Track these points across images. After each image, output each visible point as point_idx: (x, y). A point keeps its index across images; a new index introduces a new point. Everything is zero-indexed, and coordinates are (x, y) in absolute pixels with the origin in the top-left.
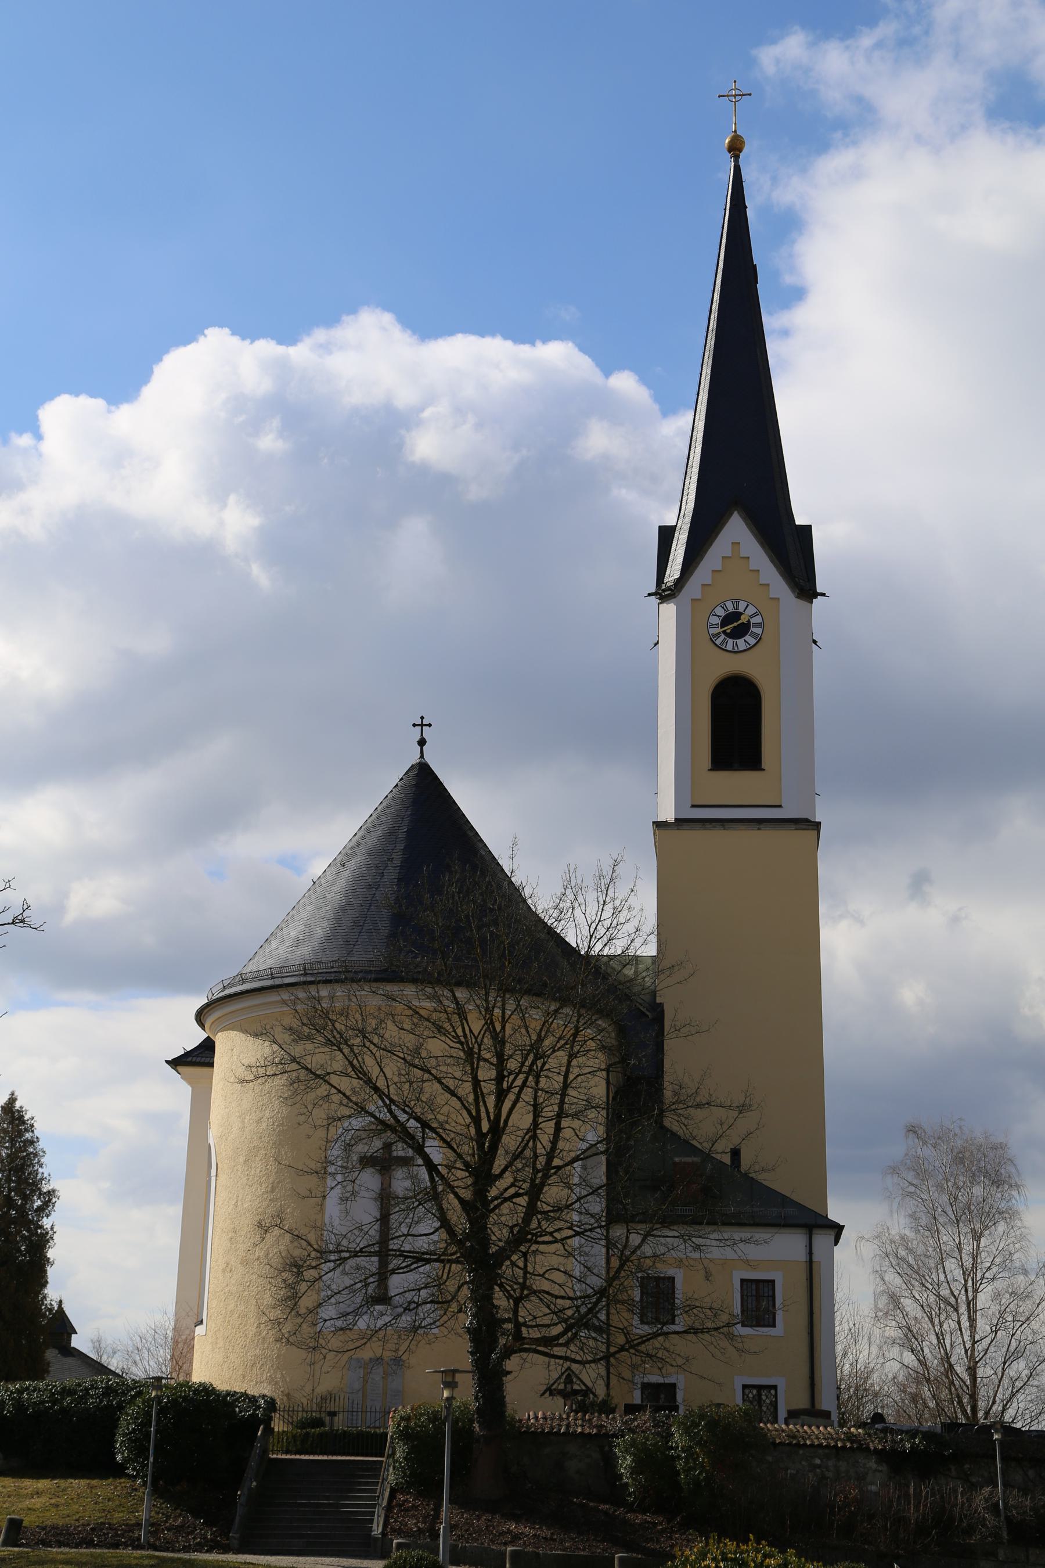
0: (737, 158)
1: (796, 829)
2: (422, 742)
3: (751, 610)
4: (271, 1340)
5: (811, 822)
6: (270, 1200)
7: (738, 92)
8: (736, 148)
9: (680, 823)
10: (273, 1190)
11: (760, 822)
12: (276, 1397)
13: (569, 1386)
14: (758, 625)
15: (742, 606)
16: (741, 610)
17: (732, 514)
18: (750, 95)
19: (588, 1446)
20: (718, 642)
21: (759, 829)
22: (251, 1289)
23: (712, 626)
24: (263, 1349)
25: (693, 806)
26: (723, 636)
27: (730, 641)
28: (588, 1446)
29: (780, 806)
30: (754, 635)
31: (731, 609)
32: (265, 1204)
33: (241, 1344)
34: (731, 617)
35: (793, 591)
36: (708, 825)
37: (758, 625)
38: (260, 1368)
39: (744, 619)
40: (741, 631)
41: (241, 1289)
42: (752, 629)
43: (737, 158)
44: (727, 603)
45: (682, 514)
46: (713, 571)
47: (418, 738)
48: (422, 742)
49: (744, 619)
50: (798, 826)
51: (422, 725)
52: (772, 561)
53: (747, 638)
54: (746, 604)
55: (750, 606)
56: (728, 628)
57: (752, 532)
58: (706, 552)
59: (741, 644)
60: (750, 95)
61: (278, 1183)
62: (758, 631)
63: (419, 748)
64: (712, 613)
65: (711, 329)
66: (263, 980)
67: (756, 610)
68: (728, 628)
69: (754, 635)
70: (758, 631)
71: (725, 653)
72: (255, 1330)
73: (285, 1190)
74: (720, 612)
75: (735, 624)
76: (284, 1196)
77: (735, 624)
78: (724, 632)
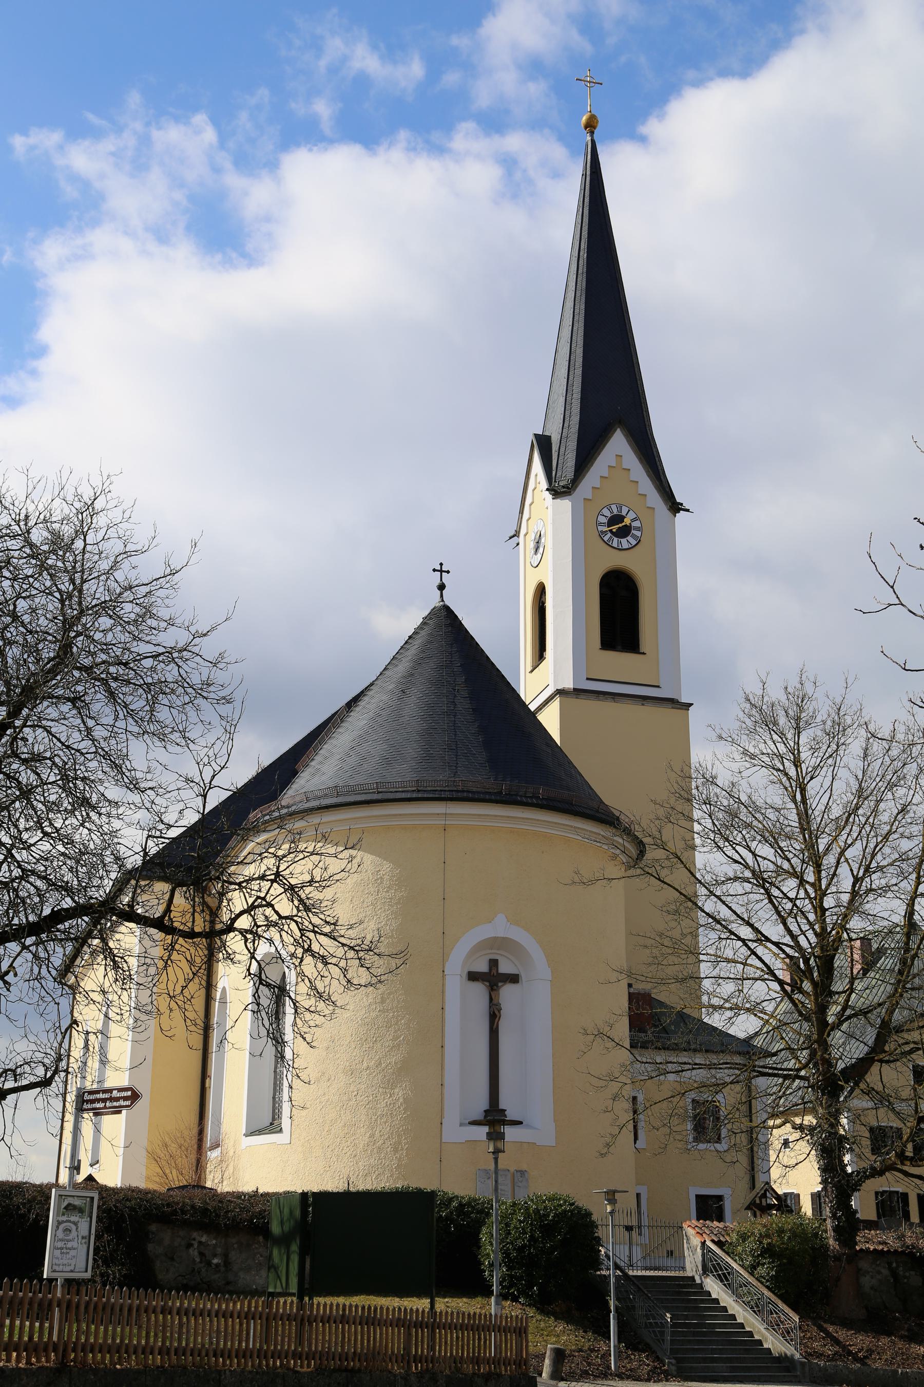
0: (592, 133)
1: (672, 708)
2: (442, 587)
3: (632, 515)
4: (388, 1150)
5: (678, 702)
6: (379, 1011)
7: (592, 80)
8: (591, 125)
9: (577, 692)
10: (383, 1001)
11: (644, 699)
12: (601, 1210)
13: (763, 1200)
14: (638, 529)
15: (624, 511)
16: (624, 513)
17: (616, 430)
18: (601, 84)
19: (878, 1263)
20: (606, 538)
21: (643, 705)
22: (358, 1098)
23: (601, 524)
24: (379, 1159)
25: (588, 679)
26: (609, 535)
27: (616, 539)
28: (878, 1263)
29: (658, 687)
30: (634, 537)
31: (615, 512)
32: (373, 1014)
33: (348, 1154)
34: (616, 519)
35: (666, 504)
36: (601, 697)
37: (638, 529)
38: (377, 1178)
39: (627, 521)
40: (624, 532)
41: (345, 1098)
42: (633, 531)
43: (592, 133)
44: (623, 507)
45: (566, 425)
46: (601, 477)
47: (438, 582)
48: (442, 587)
49: (627, 521)
50: (674, 705)
51: (441, 571)
52: (649, 476)
53: (629, 538)
54: (627, 509)
55: (631, 512)
56: (614, 528)
57: (632, 449)
58: (595, 459)
59: (624, 543)
60: (601, 84)
61: (389, 994)
62: (638, 533)
63: (439, 592)
64: (600, 513)
65: (580, 271)
66: (366, 793)
67: (635, 516)
68: (614, 528)
69: (634, 537)
70: (638, 533)
71: (611, 549)
72: (367, 1140)
73: (398, 1002)
74: (606, 512)
75: (620, 525)
76: (397, 1007)
77: (620, 525)
78: (611, 531)
